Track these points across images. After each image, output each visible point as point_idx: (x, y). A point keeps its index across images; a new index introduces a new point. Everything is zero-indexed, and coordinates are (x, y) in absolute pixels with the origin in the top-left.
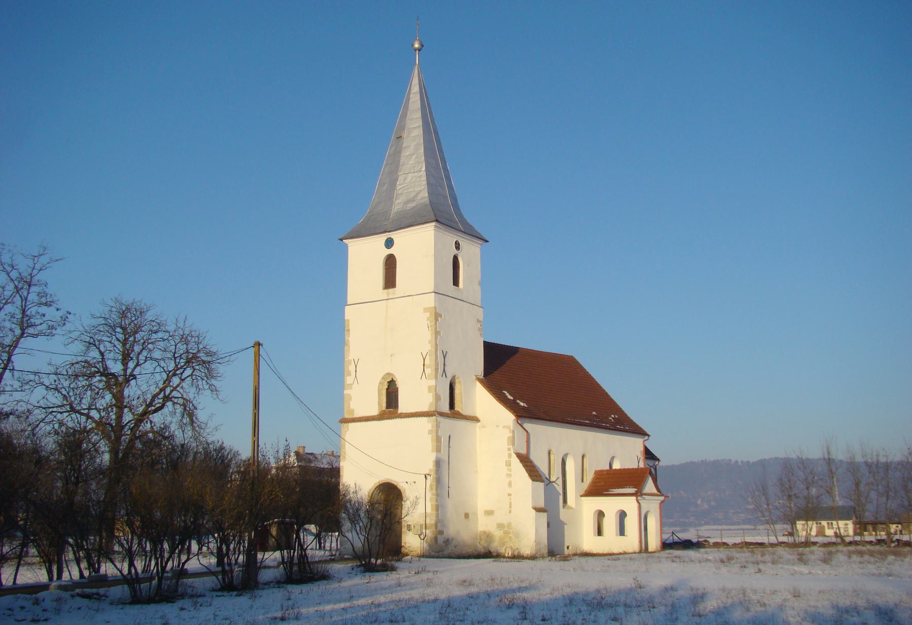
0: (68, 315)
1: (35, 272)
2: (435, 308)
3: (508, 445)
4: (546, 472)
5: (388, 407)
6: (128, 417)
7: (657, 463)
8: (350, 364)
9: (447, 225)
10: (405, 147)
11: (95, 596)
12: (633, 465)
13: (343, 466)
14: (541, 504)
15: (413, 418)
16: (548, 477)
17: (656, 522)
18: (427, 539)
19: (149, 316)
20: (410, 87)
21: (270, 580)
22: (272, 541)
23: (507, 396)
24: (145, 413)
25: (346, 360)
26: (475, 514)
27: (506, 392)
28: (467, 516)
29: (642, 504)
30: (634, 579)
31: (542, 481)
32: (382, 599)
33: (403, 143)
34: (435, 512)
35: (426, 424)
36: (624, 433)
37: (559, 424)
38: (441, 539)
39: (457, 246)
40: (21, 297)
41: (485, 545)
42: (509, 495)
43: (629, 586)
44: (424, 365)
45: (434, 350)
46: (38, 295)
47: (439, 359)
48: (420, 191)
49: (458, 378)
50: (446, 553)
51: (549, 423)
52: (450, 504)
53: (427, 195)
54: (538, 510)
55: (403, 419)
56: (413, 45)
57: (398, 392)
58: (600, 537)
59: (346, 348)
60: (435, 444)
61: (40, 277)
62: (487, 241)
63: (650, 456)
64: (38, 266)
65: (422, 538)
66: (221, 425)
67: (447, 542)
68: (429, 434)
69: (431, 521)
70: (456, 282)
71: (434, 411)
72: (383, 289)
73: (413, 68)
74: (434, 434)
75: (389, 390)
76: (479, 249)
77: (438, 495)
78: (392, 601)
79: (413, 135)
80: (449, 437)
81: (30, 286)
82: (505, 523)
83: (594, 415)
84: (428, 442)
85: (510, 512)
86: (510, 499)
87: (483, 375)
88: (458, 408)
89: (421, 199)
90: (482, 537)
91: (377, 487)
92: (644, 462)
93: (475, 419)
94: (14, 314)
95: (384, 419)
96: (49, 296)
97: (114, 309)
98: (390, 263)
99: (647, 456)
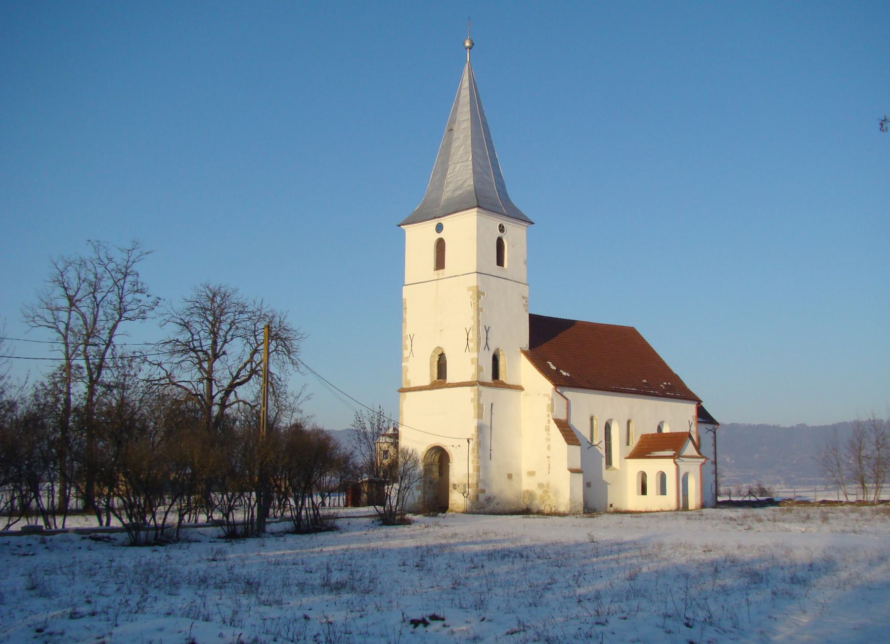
1: (130, 263)
2: (478, 287)
4: (586, 434)
5: (438, 378)
7: (716, 426)
9: (489, 210)
12: (684, 429)
14: (578, 465)
15: (458, 388)
16: (590, 441)
21: (280, 530)
24: (232, 387)
27: (550, 363)
28: (510, 476)
29: (681, 466)
31: (580, 445)
32: (354, 546)
34: (476, 473)
35: (469, 393)
37: (601, 391)
38: (482, 497)
39: (502, 229)
45: (476, 325)
46: (131, 284)
48: (467, 179)
51: (592, 391)
52: (493, 464)
53: (472, 183)
54: (573, 471)
55: (450, 389)
57: (446, 364)
61: (135, 268)
62: (532, 223)
64: (131, 260)
67: (489, 500)
68: (472, 402)
69: (472, 481)
70: (500, 262)
71: (475, 382)
72: (434, 270)
74: (476, 403)
75: (440, 363)
77: (479, 457)
81: (125, 276)
82: (545, 482)
83: (644, 383)
84: (470, 410)
85: (549, 473)
86: (549, 461)
87: (528, 347)
88: (502, 377)
90: (526, 496)
91: (429, 451)
93: (519, 388)
94: (111, 301)
96: (139, 284)
98: (440, 246)
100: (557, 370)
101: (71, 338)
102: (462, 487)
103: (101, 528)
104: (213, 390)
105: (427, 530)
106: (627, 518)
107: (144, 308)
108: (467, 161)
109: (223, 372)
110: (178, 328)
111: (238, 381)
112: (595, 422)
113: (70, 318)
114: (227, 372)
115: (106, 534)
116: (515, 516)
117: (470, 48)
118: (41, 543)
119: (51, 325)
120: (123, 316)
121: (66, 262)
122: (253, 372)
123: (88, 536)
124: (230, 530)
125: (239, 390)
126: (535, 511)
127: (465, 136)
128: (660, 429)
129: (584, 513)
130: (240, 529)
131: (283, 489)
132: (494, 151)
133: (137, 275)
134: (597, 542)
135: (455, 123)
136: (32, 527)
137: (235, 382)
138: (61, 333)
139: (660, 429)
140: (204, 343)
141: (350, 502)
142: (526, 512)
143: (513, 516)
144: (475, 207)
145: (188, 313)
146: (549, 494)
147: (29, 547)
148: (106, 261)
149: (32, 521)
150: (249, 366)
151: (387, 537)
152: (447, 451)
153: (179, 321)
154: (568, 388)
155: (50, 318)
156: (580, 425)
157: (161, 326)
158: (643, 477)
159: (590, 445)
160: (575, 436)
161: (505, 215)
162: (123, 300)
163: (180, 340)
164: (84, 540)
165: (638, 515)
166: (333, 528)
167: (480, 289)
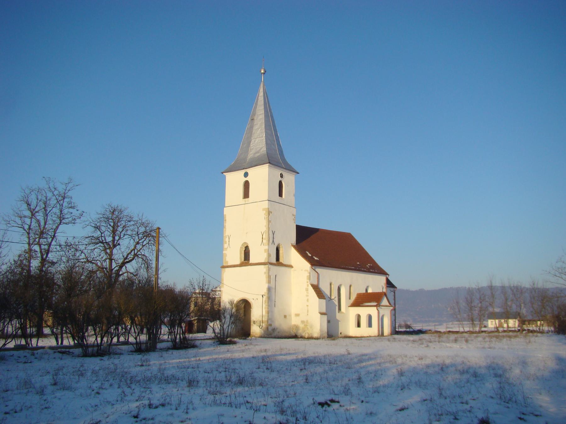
0: (83, 213)
1: (67, 191)
2: (268, 208)
6: (114, 265)
8: (226, 238)
10: (256, 124)
12: (379, 290)
14: (324, 310)
15: (258, 266)
16: (330, 297)
18: (263, 328)
19: (125, 213)
20: (259, 93)
21: (164, 347)
22: (195, 327)
23: (308, 254)
24: (124, 264)
26: (290, 316)
27: (307, 252)
28: (285, 316)
30: (347, 350)
31: (325, 299)
34: (267, 315)
35: (263, 268)
39: (282, 176)
40: (59, 204)
41: (295, 332)
42: (307, 306)
43: (344, 353)
44: (262, 238)
45: (267, 230)
46: (68, 203)
47: (270, 235)
48: (262, 147)
50: (273, 335)
51: (337, 269)
52: (276, 310)
53: (265, 149)
54: (322, 314)
55: (252, 266)
56: (260, 71)
58: (359, 328)
59: (224, 229)
60: (268, 279)
61: (70, 194)
62: (298, 173)
64: (68, 189)
65: (261, 328)
66: (167, 269)
67: (274, 330)
69: (265, 319)
70: (280, 195)
71: (267, 262)
72: (243, 199)
73: (260, 84)
74: (267, 274)
75: (246, 251)
76: (294, 178)
77: (269, 306)
81: (64, 199)
83: (358, 264)
84: (264, 279)
85: (308, 314)
86: (308, 308)
87: (295, 243)
88: (281, 260)
89: (263, 151)
90: (294, 328)
92: (386, 288)
93: (291, 266)
94: (56, 213)
95: (242, 266)
96: (73, 203)
97: (108, 210)
98: (247, 185)
99: (388, 285)
100: (312, 256)
101: (32, 235)
103: (58, 346)
104: (113, 265)
106: (353, 340)
107: (75, 217)
108: (263, 137)
109: (119, 254)
110: (93, 229)
111: (127, 260)
112: (332, 286)
113: (31, 222)
114: (121, 255)
115: (67, 350)
116: (290, 339)
117: (264, 74)
118: (32, 355)
119: (20, 226)
120: (62, 221)
121: (30, 189)
122: (136, 255)
123: (57, 351)
124: (138, 347)
125: (128, 265)
127: (261, 123)
128: (366, 290)
130: (143, 347)
131: (77, 325)
132: (277, 132)
133: (71, 198)
134: (351, 354)
135: (255, 115)
136: (19, 345)
137: (126, 261)
138: (26, 231)
139: (366, 290)
140: (107, 238)
142: (295, 337)
143: (289, 339)
144: (268, 163)
145: (99, 221)
147: (25, 358)
148: (53, 190)
149: (18, 342)
150: (133, 252)
152: (250, 302)
153: (94, 225)
154: (319, 267)
155: (20, 222)
156: (325, 288)
157: (83, 228)
158: (359, 317)
159: (330, 299)
160: (322, 294)
161: (284, 168)
162: (63, 212)
163: (94, 236)
164: (56, 353)
165: (360, 338)
166: (194, 346)
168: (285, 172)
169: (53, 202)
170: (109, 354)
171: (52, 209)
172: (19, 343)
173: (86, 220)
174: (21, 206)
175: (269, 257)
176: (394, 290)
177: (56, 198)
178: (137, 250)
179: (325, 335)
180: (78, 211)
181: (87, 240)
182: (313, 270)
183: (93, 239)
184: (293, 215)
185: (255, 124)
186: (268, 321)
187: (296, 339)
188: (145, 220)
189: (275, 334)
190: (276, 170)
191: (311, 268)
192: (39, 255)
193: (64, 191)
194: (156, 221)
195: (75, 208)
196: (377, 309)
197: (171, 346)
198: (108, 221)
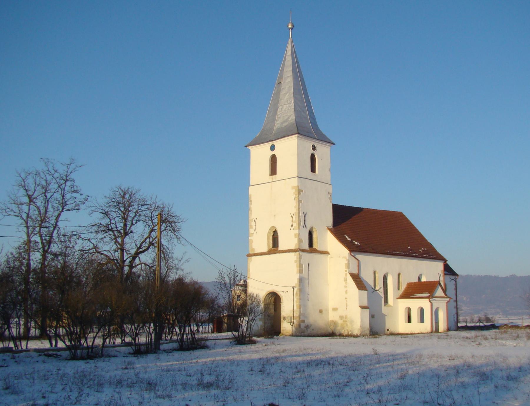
1: (69, 173)
2: (298, 186)
3: (345, 268)
5: (273, 247)
7: (457, 277)
9: (305, 136)
11: (55, 356)
13: (249, 283)
14: (366, 303)
15: (289, 253)
17: (444, 314)
23: (347, 239)
24: (137, 254)
25: (250, 219)
26: (327, 310)
27: (346, 236)
28: (321, 311)
31: (367, 290)
32: (218, 358)
33: (281, 87)
34: (298, 309)
35: (293, 256)
36: (426, 259)
39: (314, 148)
44: (292, 221)
46: (70, 187)
47: (301, 218)
48: (291, 115)
49: (315, 228)
50: (306, 333)
52: (310, 304)
53: (294, 118)
54: (362, 307)
55: (281, 254)
56: (288, 26)
59: (250, 212)
60: (299, 268)
61: (72, 176)
62: (334, 144)
63: (452, 273)
64: (70, 171)
67: (307, 327)
69: (296, 314)
70: (313, 170)
71: (298, 249)
72: (270, 176)
75: (274, 237)
77: (300, 299)
78: (222, 360)
79: (287, 81)
80: (308, 264)
81: (66, 182)
82: (344, 315)
83: (409, 249)
84: (294, 268)
85: (347, 308)
86: (347, 301)
87: (332, 226)
88: (315, 246)
89: (291, 120)
90: (332, 324)
93: (327, 253)
94: (56, 198)
96: (75, 187)
98: (273, 160)
100: (351, 241)
101: (30, 223)
102: (289, 318)
103: (52, 348)
105: (266, 347)
106: (398, 338)
107: (78, 202)
110: (101, 216)
111: (141, 250)
112: (377, 275)
113: (29, 210)
114: (133, 244)
115: (55, 352)
117: (292, 29)
118: (12, 358)
119: (17, 214)
120: (64, 208)
121: (27, 173)
122: (151, 244)
124: (137, 349)
125: (142, 256)
126: (338, 334)
128: (419, 279)
129: (370, 335)
130: (143, 348)
131: (171, 322)
132: (308, 97)
133: (74, 181)
134: (379, 354)
135: (282, 78)
137: (139, 251)
139: (419, 279)
140: (118, 225)
141: (215, 330)
142: (332, 335)
146: (347, 323)
147: (4, 361)
148: (53, 172)
151: (240, 352)
152: (279, 295)
153: (101, 211)
154: (359, 253)
156: (367, 277)
157: (90, 214)
158: (409, 311)
159: (374, 290)
160: (363, 284)
162: (64, 197)
166: (205, 347)
167: (300, 188)
168: (317, 144)
169: (53, 186)
170: (102, 356)
171: (54, 194)
172: (7, 346)
173: (92, 205)
174: (18, 192)
175: (300, 243)
176: (455, 278)
177: (57, 181)
178: (152, 238)
179: (367, 332)
180: (82, 196)
181: (95, 228)
182: (352, 256)
183: (101, 227)
184: (328, 192)
185: (282, 88)
186: (299, 317)
187: (331, 337)
188: (160, 203)
189: (309, 331)
190: (306, 140)
191: (349, 254)
192: (40, 246)
193: (66, 173)
194: (173, 204)
195: (78, 193)
196: (430, 301)
197: (178, 347)
198: (118, 206)
